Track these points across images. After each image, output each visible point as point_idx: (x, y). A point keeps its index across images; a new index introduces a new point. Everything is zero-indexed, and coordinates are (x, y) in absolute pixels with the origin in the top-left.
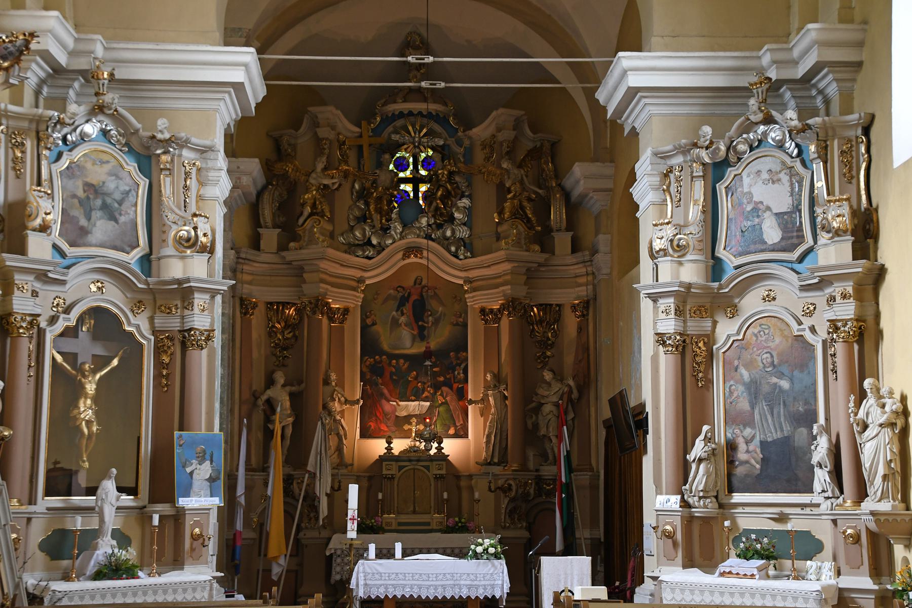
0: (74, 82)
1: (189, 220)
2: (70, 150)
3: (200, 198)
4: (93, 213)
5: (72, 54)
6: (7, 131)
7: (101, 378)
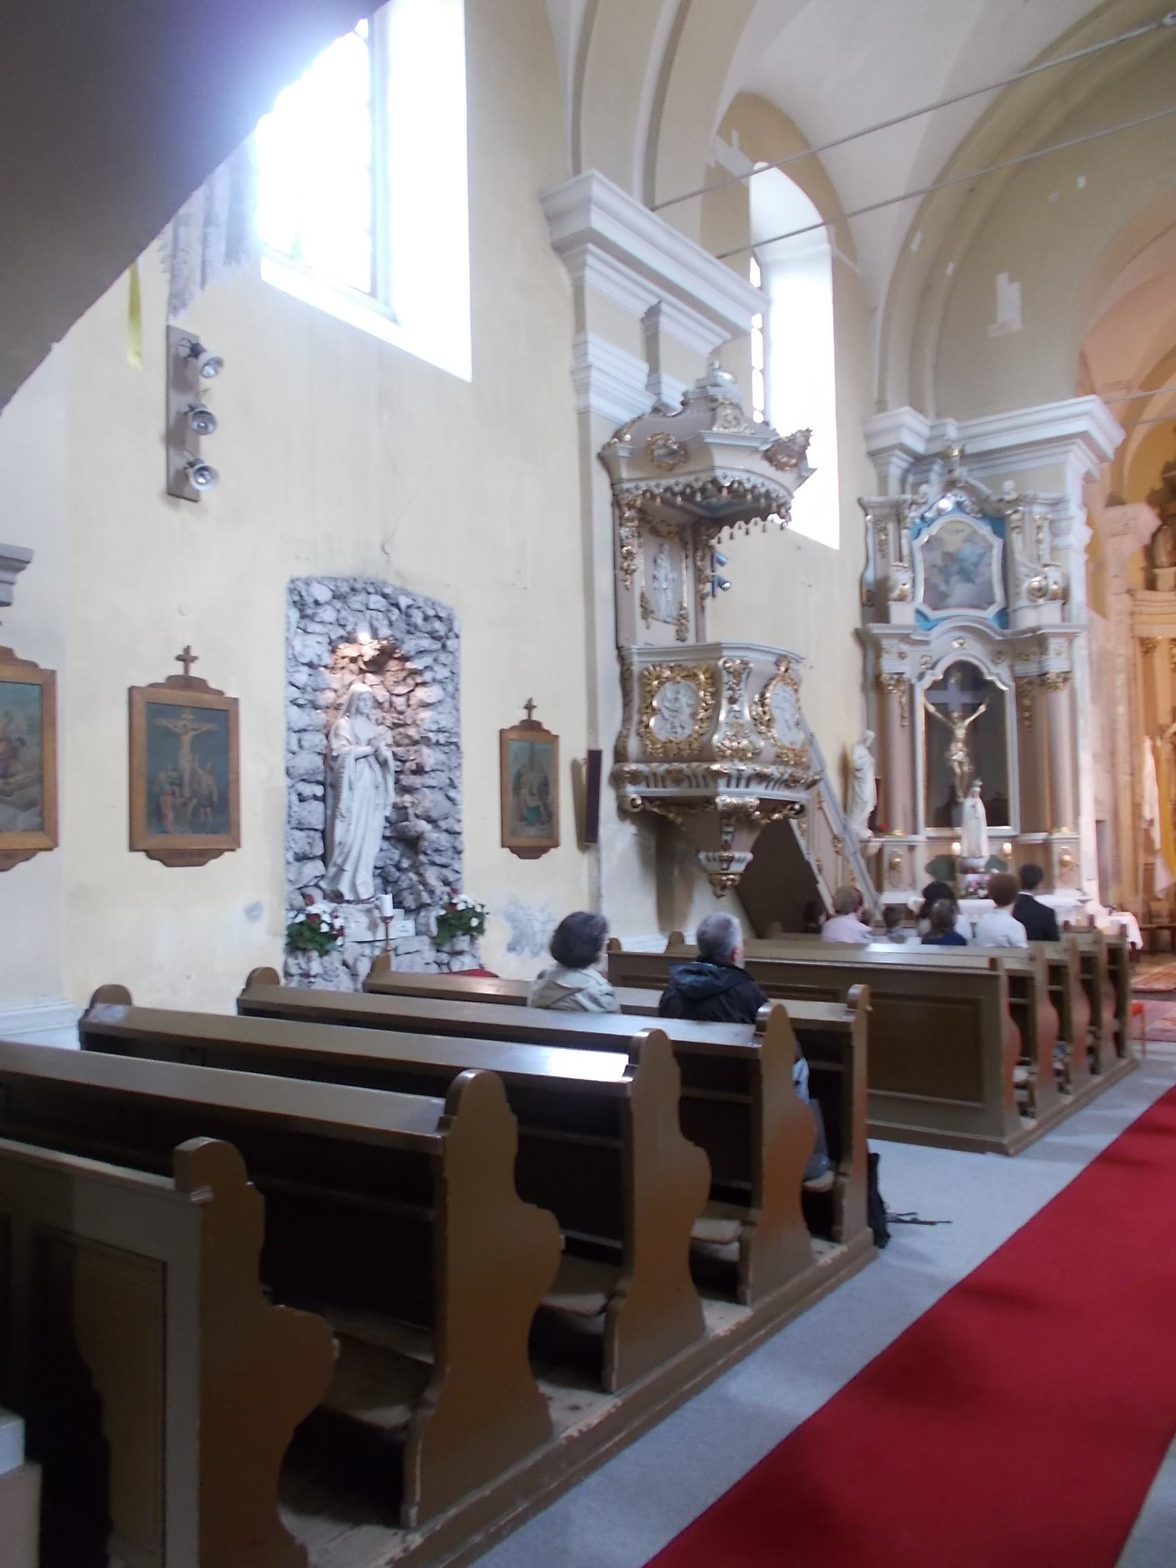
3: (1054, 549)
5: (929, 440)
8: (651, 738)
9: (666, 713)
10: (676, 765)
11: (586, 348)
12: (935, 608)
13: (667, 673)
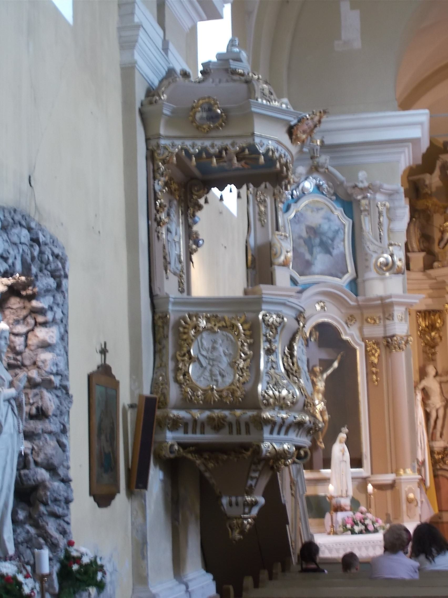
2: (296, 202)
7: (328, 377)
8: (190, 385)
10: (217, 413)
11: (134, 8)
12: (301, 274)
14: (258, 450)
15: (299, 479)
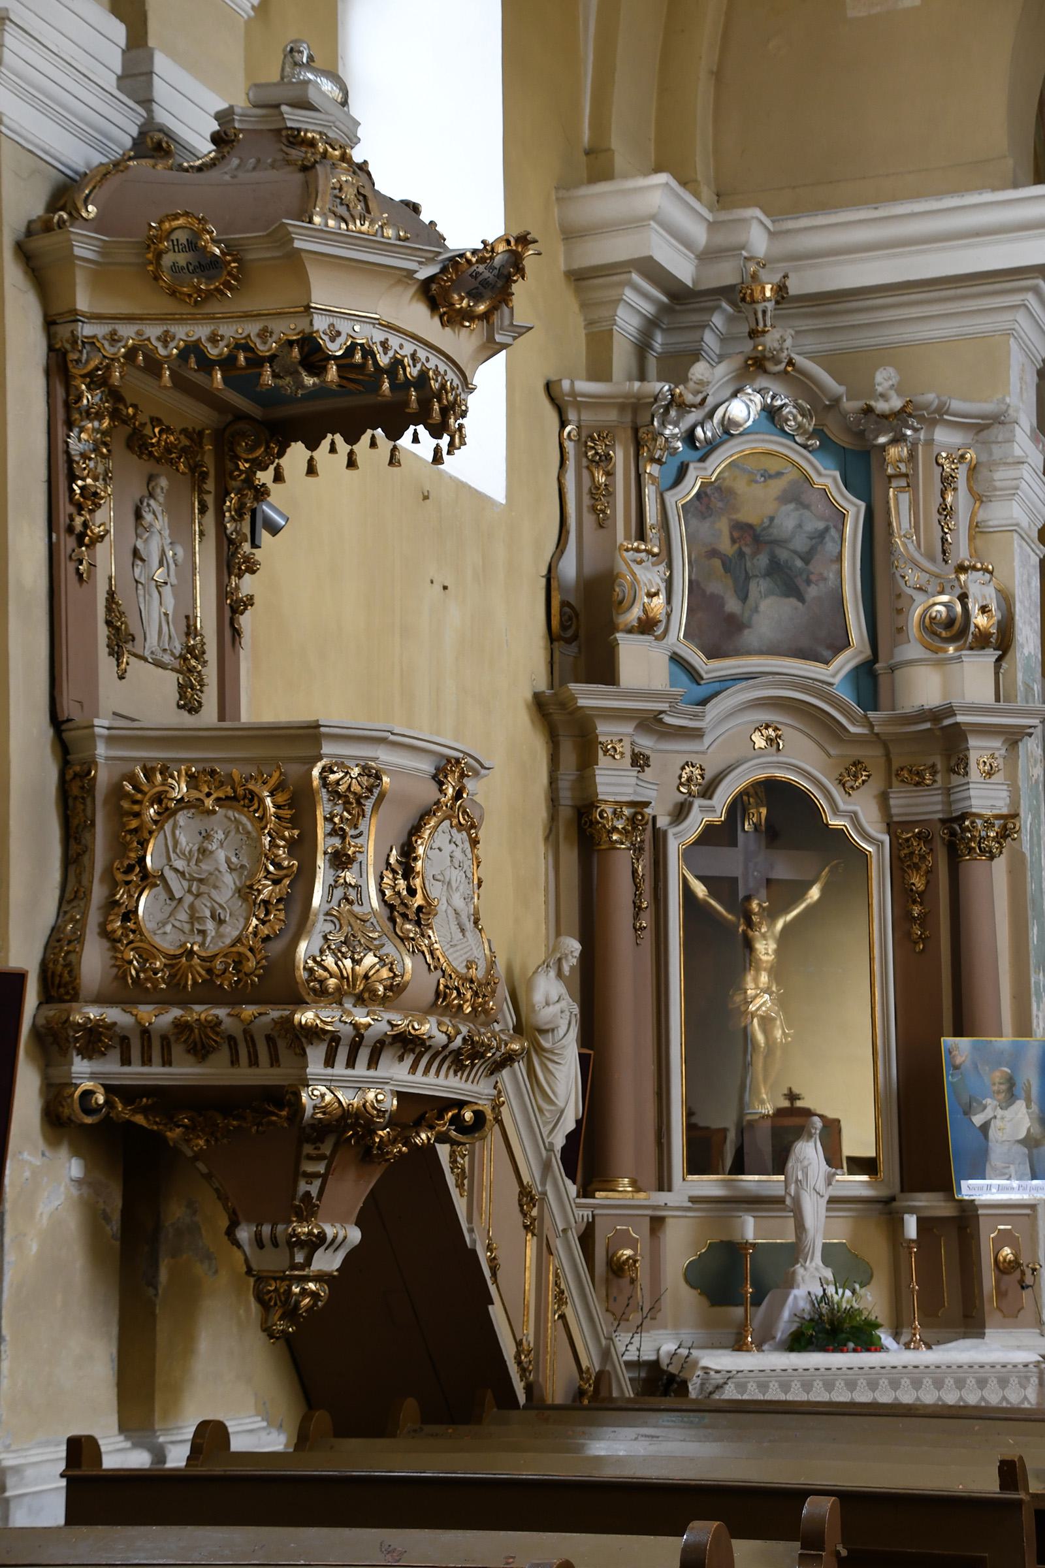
0: (712, 315)
1: (950, 581)
2: (703, 459)
3: (977, 529)
4: (753, 586)
5: (706, 257)
6: (579, 434)
7: (786, 927)
9: (178, 886)
10: (200, 1012)
12: (712, 653)
13: (181, 789)
14: (298, 1107)
15: (549, 1189)
